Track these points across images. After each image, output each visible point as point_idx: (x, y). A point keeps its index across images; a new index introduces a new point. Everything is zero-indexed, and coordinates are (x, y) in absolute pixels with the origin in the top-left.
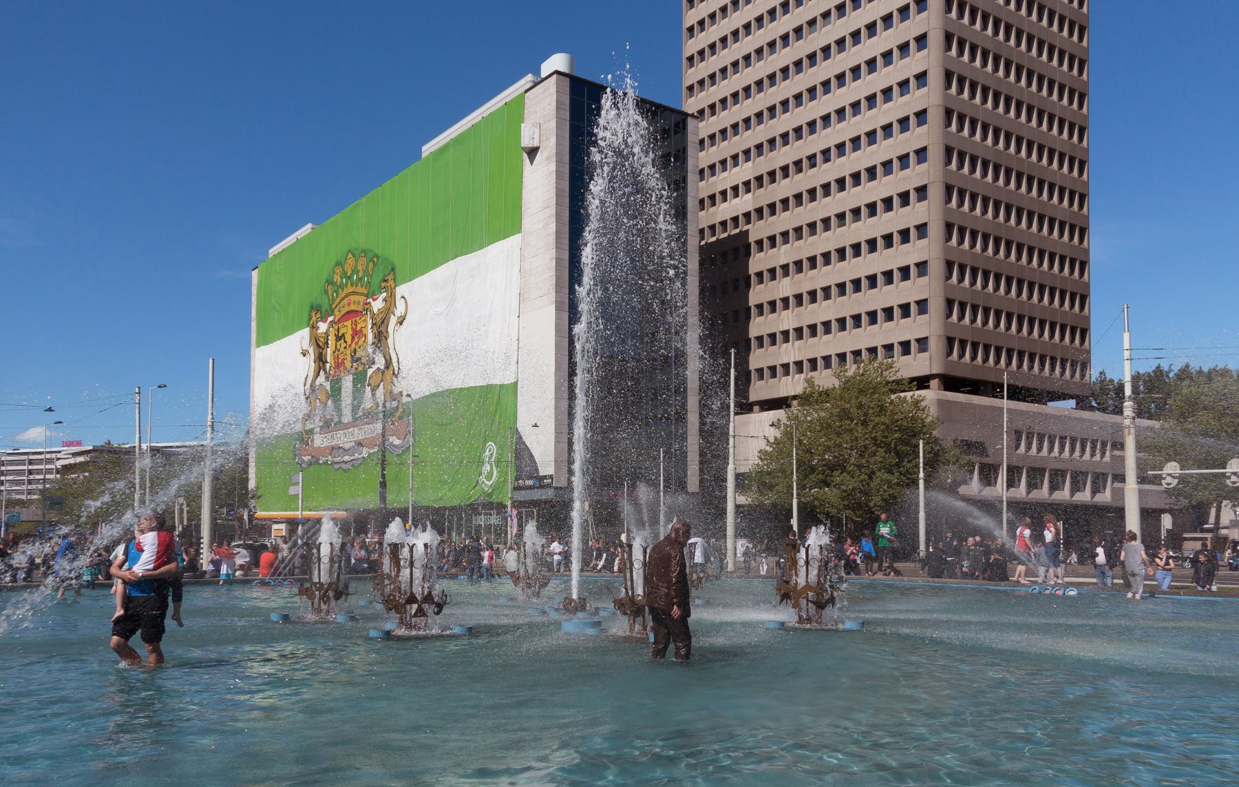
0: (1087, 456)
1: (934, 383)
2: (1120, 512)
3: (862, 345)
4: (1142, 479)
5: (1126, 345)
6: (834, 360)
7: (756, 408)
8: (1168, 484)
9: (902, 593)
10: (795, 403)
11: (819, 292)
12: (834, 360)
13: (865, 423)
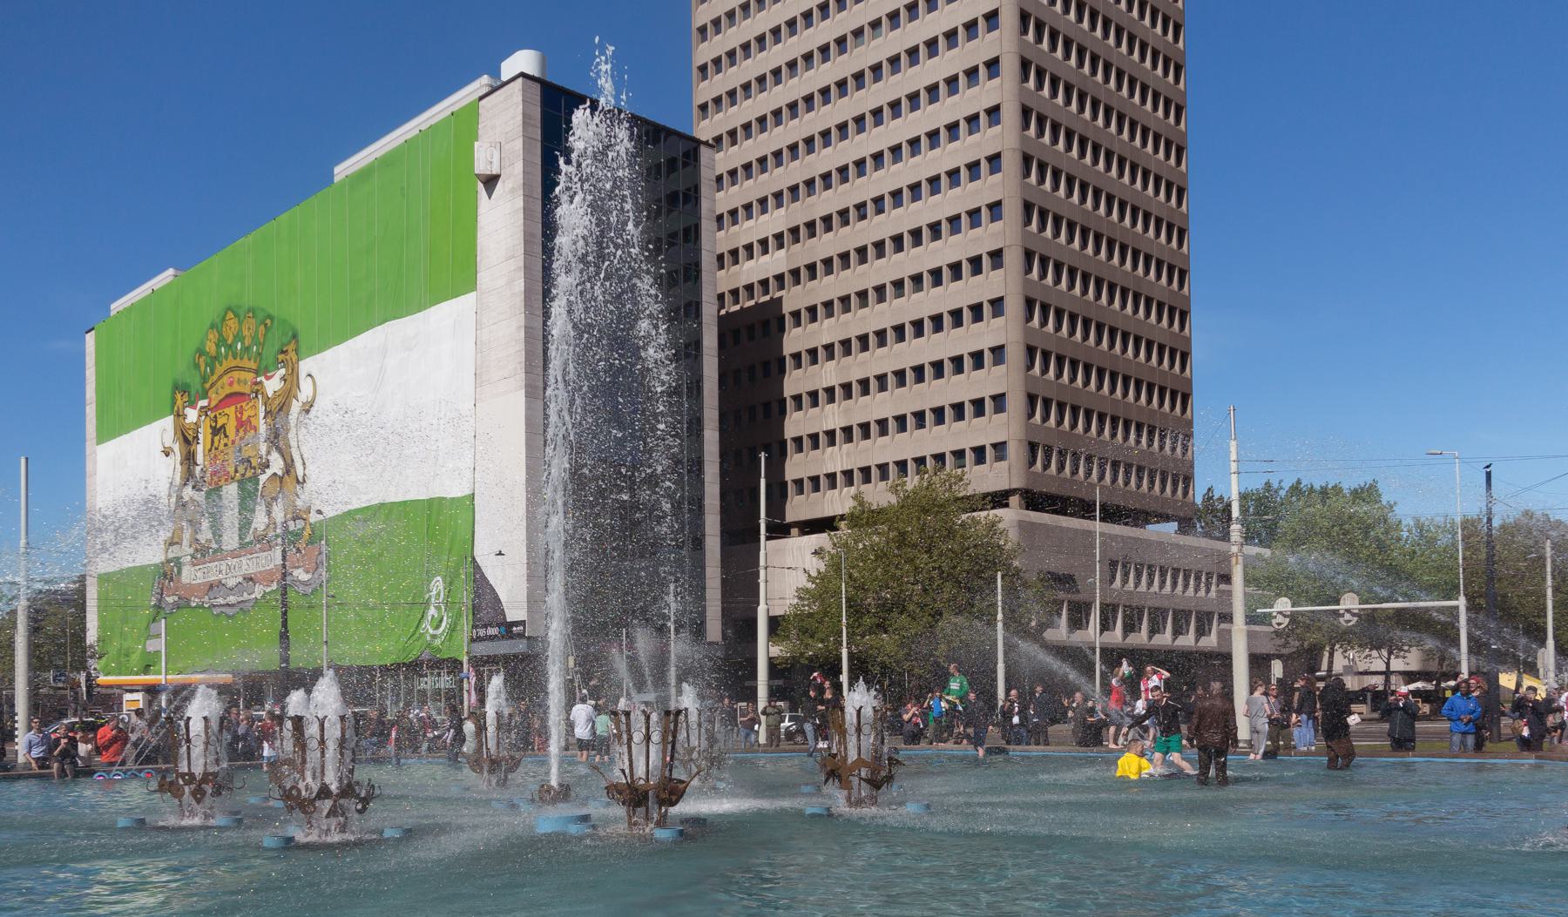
1: (1014, 500)
10: (843, 524)
11: (805, 397)
12: (893, 470)
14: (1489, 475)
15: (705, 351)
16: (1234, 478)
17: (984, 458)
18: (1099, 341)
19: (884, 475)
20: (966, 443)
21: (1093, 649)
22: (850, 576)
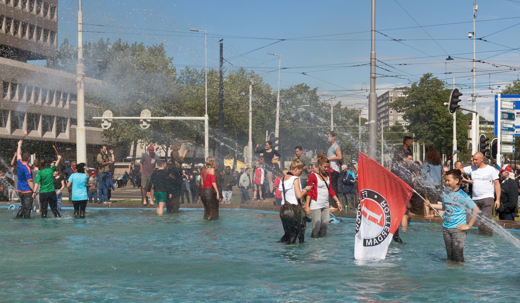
0: (54, 104)
2: (73, 146)
4: (89, 122)
5: (80, 20)
8: (105, 126)
16: (80, 34)
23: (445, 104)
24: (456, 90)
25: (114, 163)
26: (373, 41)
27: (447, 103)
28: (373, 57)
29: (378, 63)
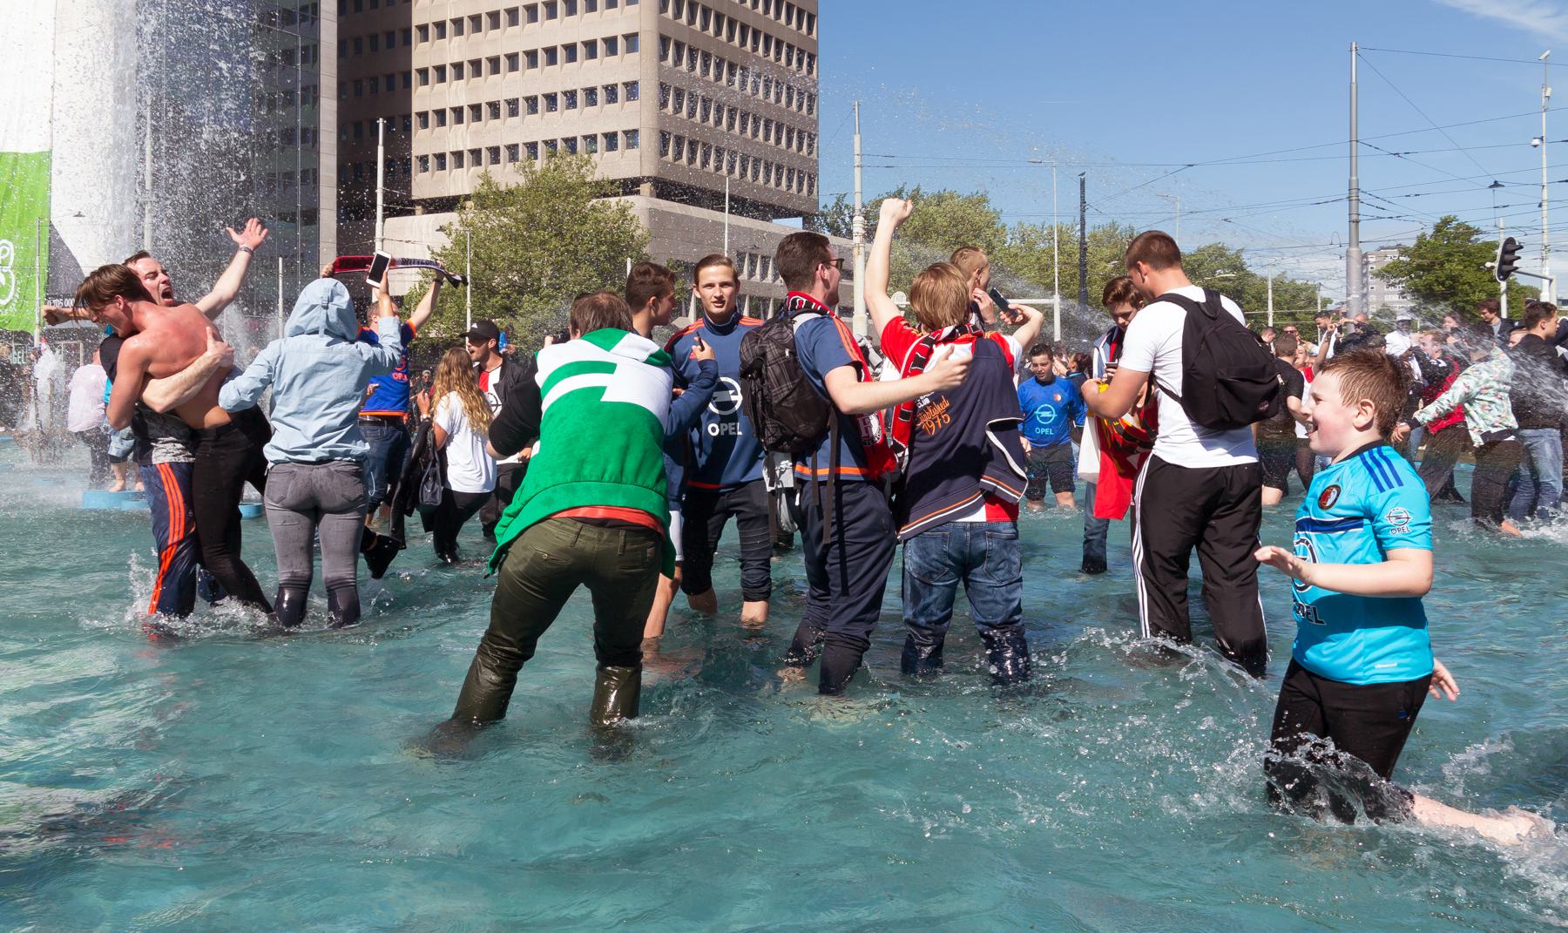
1: (645, 188)
3: (520, 138)
6: (522, 152)
7: (419, 209)
9: (30, 574)
10: (469, 204)
11: (431, 72)
12: (522, 152)
13: (559, 234)
14: (1083, 183)
15: (323, 14)
16: (857, 171)
17: (616, 145)
18: (731, 37)
19: (513, 157)
20: (599, 129)
21: (731, 208)
22: (476, 254)
23: (1488, 264)
24: (1510, 241)
25: (1502, 319)
26: (1354, 159)
27: (1493, 264)
28: (1354, 186)
29: (1362, 197)
